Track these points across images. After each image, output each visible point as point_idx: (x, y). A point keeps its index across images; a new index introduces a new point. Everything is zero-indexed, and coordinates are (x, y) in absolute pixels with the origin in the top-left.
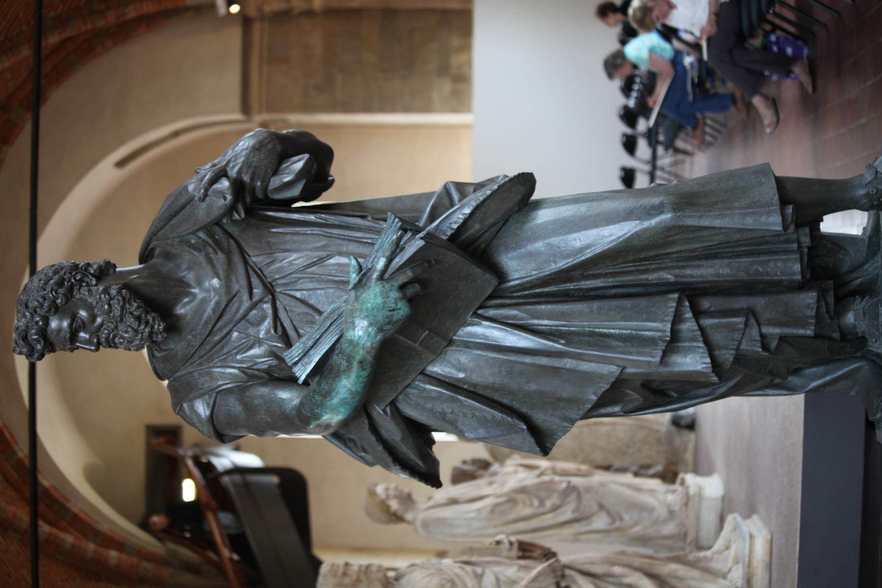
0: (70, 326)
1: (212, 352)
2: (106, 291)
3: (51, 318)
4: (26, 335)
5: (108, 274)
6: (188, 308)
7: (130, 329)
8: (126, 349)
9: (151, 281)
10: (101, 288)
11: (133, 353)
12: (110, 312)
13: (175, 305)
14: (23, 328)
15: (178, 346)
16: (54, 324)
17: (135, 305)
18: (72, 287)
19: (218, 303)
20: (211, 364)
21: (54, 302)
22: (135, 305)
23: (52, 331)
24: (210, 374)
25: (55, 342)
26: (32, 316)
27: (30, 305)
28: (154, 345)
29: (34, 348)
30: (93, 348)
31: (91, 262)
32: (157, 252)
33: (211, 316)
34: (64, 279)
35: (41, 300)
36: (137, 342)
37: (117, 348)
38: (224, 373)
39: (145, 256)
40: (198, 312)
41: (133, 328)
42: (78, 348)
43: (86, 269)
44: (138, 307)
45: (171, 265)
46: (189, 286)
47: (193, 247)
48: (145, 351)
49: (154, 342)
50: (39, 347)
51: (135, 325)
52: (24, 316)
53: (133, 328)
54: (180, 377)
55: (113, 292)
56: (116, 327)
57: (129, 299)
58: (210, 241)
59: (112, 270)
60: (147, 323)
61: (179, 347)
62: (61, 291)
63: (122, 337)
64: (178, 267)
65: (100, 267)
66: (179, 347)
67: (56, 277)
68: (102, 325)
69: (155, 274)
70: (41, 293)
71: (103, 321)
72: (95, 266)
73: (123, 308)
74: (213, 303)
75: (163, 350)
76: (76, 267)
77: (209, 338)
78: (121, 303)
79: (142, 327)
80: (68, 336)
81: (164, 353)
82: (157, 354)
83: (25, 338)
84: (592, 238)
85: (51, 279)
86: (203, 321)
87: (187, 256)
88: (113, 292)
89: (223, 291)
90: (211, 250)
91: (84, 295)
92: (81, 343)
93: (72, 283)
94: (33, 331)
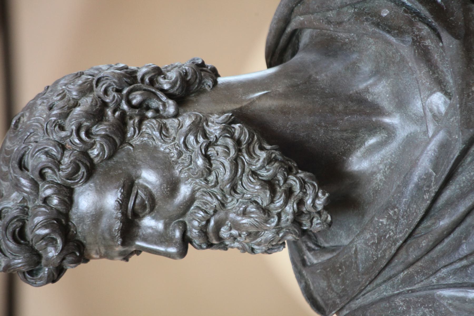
0: (123, 204)
1: (433, 254)
2: (199, 128)
3: (78, 189)
5: (200, 91)
6: (377, 157)
7: (251, 208)
8: (244, 250)
9: (293, 103)
10: (188, 122)
13: (348, 152)
14: (15, 212)
15: (355, 240)
16: (85, 201)
17: (263, 155)
19: (444, 147)
21: (85, 153)
22: (263, 155)
23: (82, 219)
25: (89, 240)
26: (35, 185)
27: (30, 162)
28: (302, 237)
29: (40, 256)
30: (172, 250)
31: (162, 66)
32: (305, 38)
33: (428, 176)
34: (105, 105)
35: (54, 151)
36: (269, 235)
37: (225, 248)
38: (463, 300)
39: (275, 56)
40: (400, 167)
42: (138, 252)
43: (152, 82)
44: (270, 161)
45: (336, 66)
46: (377, 110)
47: (383, 24)
49: (304, 232)
50: (52, 253)
51: (264, 198)
52: (17, 186)
55: (214, 129)
56: (223, 205)
57: (249, 144)
58: (424, 11)
59: (210, 83)
60: (289, 192)
61: (359, 244)
62: (100, 130)
63: (236, 225)
64: (353, 69)
65: (183, 76)
66: (359, 244)
68: (192, 199)
69: (304, 87)
70: (55, 137)
71: (193, 192)
72: (173, 75)
73: (235, 162)
74: (432, 147)
75: (324, 249)
76: (130, 76)
77: (427, 223)
78: (233, 153)
79: (279, 202)
80: (118, 225)
81: (328, 256)
82: (311, 258)
84: (308, 35)
85: (76, 105)
86: (411, 186)
87: (372, 46)
88: (214, 129)
89: (455, 120)
90: (425, 30)
91: (151, 137)
92: (145, 240)
93: (123, 113)
94: (39, 219)
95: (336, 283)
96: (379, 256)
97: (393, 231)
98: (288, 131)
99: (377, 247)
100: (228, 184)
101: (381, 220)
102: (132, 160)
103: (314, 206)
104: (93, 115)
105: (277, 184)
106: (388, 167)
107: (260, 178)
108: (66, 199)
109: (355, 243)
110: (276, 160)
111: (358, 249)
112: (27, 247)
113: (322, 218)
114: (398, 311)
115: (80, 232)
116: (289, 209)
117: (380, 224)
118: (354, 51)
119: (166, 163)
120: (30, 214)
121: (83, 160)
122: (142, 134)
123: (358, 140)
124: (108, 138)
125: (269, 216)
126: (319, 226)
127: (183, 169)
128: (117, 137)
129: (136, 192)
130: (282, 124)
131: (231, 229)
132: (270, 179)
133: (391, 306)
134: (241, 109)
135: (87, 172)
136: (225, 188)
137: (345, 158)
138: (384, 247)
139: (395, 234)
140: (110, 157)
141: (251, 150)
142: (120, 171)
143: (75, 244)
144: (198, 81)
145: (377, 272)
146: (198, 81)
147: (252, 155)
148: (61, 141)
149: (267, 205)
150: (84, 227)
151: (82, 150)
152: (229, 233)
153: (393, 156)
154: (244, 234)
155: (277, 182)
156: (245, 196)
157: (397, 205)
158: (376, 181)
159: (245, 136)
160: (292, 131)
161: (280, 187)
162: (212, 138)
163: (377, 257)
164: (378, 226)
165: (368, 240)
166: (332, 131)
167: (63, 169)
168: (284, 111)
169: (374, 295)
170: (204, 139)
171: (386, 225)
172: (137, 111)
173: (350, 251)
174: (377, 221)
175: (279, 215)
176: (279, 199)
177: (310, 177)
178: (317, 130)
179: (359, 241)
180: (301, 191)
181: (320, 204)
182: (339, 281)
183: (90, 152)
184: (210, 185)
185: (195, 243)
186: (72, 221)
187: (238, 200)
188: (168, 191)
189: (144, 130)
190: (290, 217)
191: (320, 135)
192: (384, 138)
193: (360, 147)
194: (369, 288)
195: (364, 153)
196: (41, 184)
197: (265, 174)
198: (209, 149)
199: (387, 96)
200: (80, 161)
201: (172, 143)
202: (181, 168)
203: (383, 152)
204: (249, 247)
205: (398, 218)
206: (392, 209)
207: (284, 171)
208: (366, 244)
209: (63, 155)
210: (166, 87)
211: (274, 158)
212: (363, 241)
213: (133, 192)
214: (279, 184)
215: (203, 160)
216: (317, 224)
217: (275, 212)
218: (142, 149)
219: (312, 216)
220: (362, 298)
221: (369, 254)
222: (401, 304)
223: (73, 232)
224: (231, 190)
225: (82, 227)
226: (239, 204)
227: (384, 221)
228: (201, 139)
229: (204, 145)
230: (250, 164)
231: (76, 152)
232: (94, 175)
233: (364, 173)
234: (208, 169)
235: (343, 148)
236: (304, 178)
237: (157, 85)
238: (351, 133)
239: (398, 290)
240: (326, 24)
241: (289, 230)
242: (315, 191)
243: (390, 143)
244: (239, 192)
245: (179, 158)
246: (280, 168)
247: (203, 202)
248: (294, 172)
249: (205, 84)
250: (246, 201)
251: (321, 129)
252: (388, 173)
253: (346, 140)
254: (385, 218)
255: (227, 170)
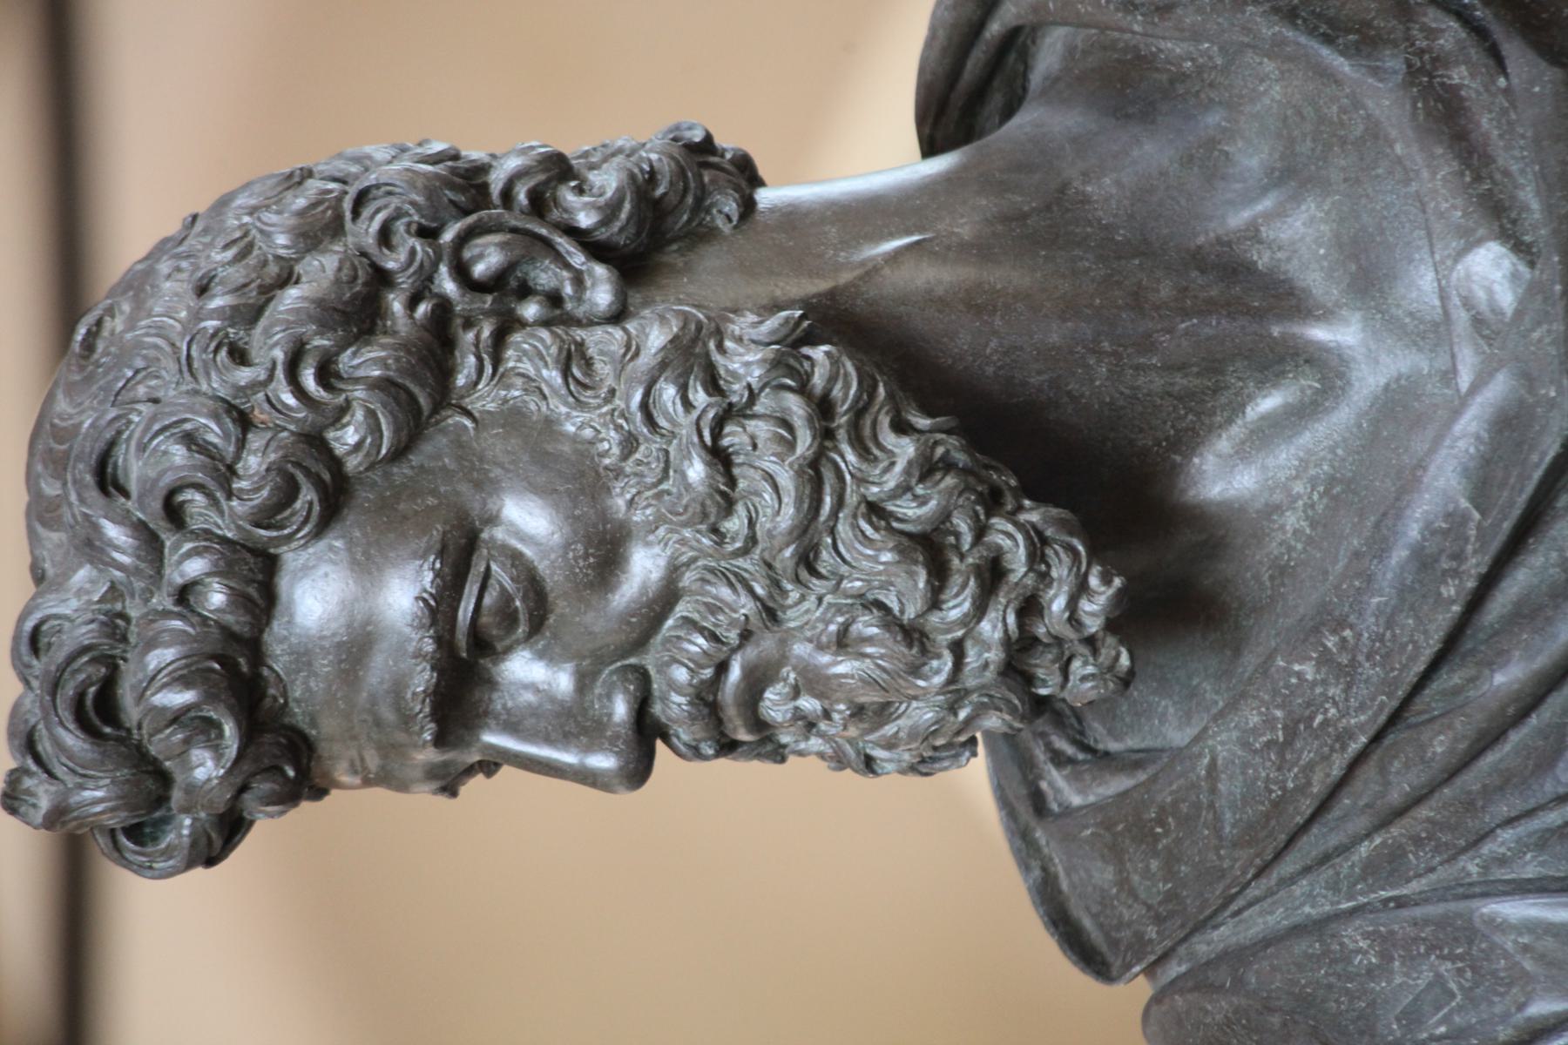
0: (440, 609)
1: (1471, 780)
2: (692, 357)
3: (292, 559)
4: (108, 688)
5: (700, 235)
6: (1284, 458)
7: (865, 625)
9: (1007, 276)
10: (656, 339)
11: (894, 788)
12: (728, 506)
13: (1188, 440)
14: (84, 633)
15: (1210, 731)
16: (315, 596)
17: (905, 449)
18: (440, 336)
20: (1471, 866)
21: (315, 441)
22: (905, 449)
23: (303, 657)
24: (1461, 939)
25: (326, 729)
26: (150, 544)
27: (134, 468)
28: (1031, 709)
29: (164, 779)
30: (603, 762)
31: (571, 148)
32: (1048, 57)
33: (1456, 520)
34: (382, 279)
35: (214, 433)
36: (922, 714)
37: (778, 754)
40: (1362, 490)
41: (889, 619)
42: (489, 766)
43: (540, 204)
44: (927, 468)
45: (1152, 153)
46: (1287, 299)
48: (975, 775)
49: (1040, 706)
50: (205, 768)
51: (907, 592)
52: (91, 547)
53: (889, 619)
54: (1237, 957)
55: (744, 363)
56: (771, 614)
57: (859, 412)
59: (731, 206)
60: (992, 574)
61: (1224, 743)
62: (366, 362)
63: (812, 681)
64: (1209, 161)
65: (642, 186)
67: (321, 271)
68: (667, 596)
69: (1043, 221)
70: (216, 384)
71: (674, 570)
72: (607, 180)
73: (813, 473)
74: (1470, 425)
75: (1104, 760)
76: (465, 185)
77: (1450, 678)
78: (805, 442)
79: (957, 607)
80: (422, 679)
81: (1118, 784)
82: (1061, 787)
83: (99, 711)
85: (287, 278)
86: (1399, 555)
88: (744, 363)
90: (1450, 35)
91: (534, 387)
93: (443, 307)
94: (163, 656)
95: (1146, 873)
96: (1291, 785)
97: (1335, 704)
98: (990, 370)
99: (1281, 755)
100: (788, 545)
101: (1297, 667)
102: (471, 461)
103: (1074, 620)
104: (344, 312)
105: (952, 545)
106: (1321, 489)
107: (895, 525)
108: (252, 591)
109: (1210, 742)
110: (948, 465)
111: (1220, 762)
112: (123, 749)
113: (1101, 659)
114: (1350, 969)
115: (297, 701)
116: (990, 628)
117: (1294, 680)
118: (1211, 100)
119: (582, 474)
120: (133, 639)
121: (308, 463)
122: (503, 375)
123: (1223, 400)
124: (393, 390)
125: (924, 651)
126: (1089, 685)
127: (639, 493)
128: (422, 386)
129: (482, 569)
130: (969, 344)
131: (796, 693)
132: (929, 528)
133: (1326, 952)
134: (832, 294)
135: (320, 501)
136: (780, 557)
137: (1178, 458)
138: (1306, 757)
139: (1344, 714)
140: (399, 453)
141: (867, 431)
142: (431, 501)
143: (283, 740)
144: (690, 200)
145: (1283, 837)
146: (690, 200)
147: (867, 451)
148: (235, 398)
149: (918, 616)
150: (312, 684)
151: (307, 429)
152: (791, 705)
153: (1340, 452)
154: (840, 712)
155: (952, 539)
156: (846, 584)
157: (1352, 619)
158: (1280, 536)
159: (847, 386)
160: (1000, 368)
161: (962, 557)
162: (737, 393)
163: (1284, 789)
164: (1287, 686)
165: (1255, 731)
166: (1137, 368)
167: (241, 490)
168: (977, 303)
169: (1271, 913)
170: (709, 395)
171: (1314, 684)
172: (489, 299)
173: (1194, 769)
174: (1285, 669)
175: (958, 649)
176: (957, 595)
177: (1062, 524)
178: (1087, 366)
179: (1224, 736)
180: (1031, 569)
181: (1093, 614)
182: (1154, 865)
183: (331, 435)
184: (730, 548)
185: (678, 738)
186: (270, 662)
187: (820, 600)
188: (589, 566)
189: (511, 364)
190: (995, 656)
191: (1096, 382)
192: (1309, 392)
193: (1230, 421)
194: (1254, 891)
195: (1243, 443)
196: (169, 540)
197: (910, 513)
198: (727, 429)
199: (1322, 251)
200: (298, 465)
201: (604, 409)
202: (634, 491)
203: (1306, 439)
204: (858, 753)
205: (1353, 659)
206: (1334, 632)
207: (976, 502)
208: (1245, 745)
209: (242, 444)
210: (585, 220)
211: (943, 458)
212: (1235, 734)
213: (473, 571)
214: (957, 547)
215: (707, 464)
216: (1084, 679)
217: (944, 639)
218: (503, 426)
219: (1067, 654)
220: (1231, 922)
221: (1257, 779)
222: (1363, 944)
223: (275, 699)
224: (797, 564)
225: (305, 683)
226: (824, 613)
227: (1308, 670)
228: (700, 397)
229: (711, 414)
230: (861, 481)
231: (285, 434)
232: (346, 511)
233: (1242, 509)
234: (723, 494)
235: (1173, 427)
236: (1040, 526)
237: (555, 214)
238: (1198, 374)
239: (1351, 898)
240: (1117, 10)
241: (990, 696)
242: (1079, 569)
243: (1327, 411)
244: (823, 571)
245: (625, 457)
246: (960, 495)
247: (706, 604)
248: (1009, 507)
249: (714, 211)
250: (849, 601)
251: (1099, 361)
252: (1320, 508)
253: (1180, 398)
254: (1311, 658)
255: (785, 500)
